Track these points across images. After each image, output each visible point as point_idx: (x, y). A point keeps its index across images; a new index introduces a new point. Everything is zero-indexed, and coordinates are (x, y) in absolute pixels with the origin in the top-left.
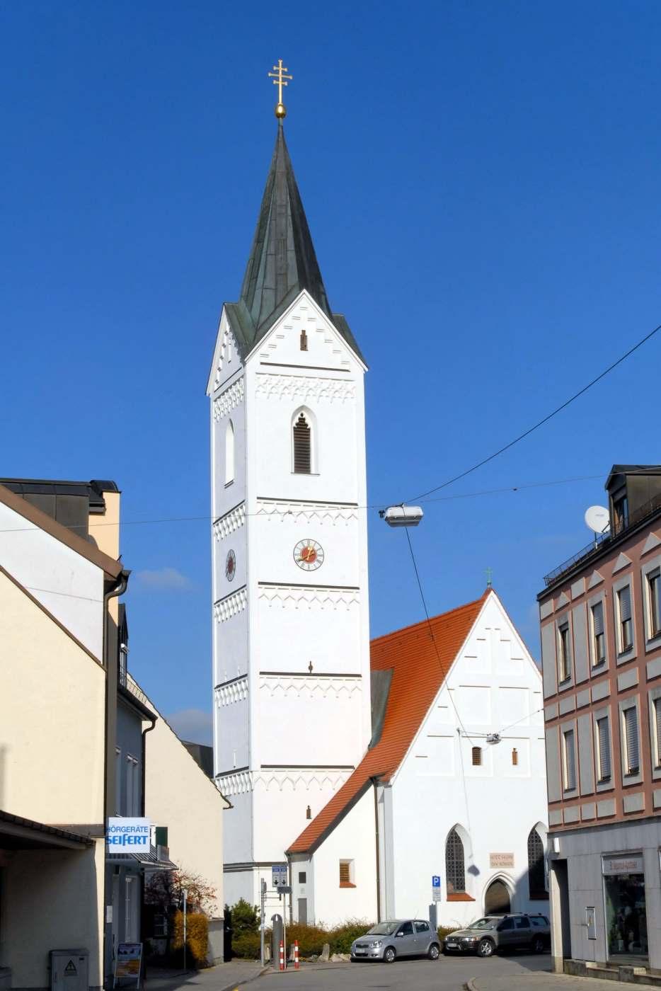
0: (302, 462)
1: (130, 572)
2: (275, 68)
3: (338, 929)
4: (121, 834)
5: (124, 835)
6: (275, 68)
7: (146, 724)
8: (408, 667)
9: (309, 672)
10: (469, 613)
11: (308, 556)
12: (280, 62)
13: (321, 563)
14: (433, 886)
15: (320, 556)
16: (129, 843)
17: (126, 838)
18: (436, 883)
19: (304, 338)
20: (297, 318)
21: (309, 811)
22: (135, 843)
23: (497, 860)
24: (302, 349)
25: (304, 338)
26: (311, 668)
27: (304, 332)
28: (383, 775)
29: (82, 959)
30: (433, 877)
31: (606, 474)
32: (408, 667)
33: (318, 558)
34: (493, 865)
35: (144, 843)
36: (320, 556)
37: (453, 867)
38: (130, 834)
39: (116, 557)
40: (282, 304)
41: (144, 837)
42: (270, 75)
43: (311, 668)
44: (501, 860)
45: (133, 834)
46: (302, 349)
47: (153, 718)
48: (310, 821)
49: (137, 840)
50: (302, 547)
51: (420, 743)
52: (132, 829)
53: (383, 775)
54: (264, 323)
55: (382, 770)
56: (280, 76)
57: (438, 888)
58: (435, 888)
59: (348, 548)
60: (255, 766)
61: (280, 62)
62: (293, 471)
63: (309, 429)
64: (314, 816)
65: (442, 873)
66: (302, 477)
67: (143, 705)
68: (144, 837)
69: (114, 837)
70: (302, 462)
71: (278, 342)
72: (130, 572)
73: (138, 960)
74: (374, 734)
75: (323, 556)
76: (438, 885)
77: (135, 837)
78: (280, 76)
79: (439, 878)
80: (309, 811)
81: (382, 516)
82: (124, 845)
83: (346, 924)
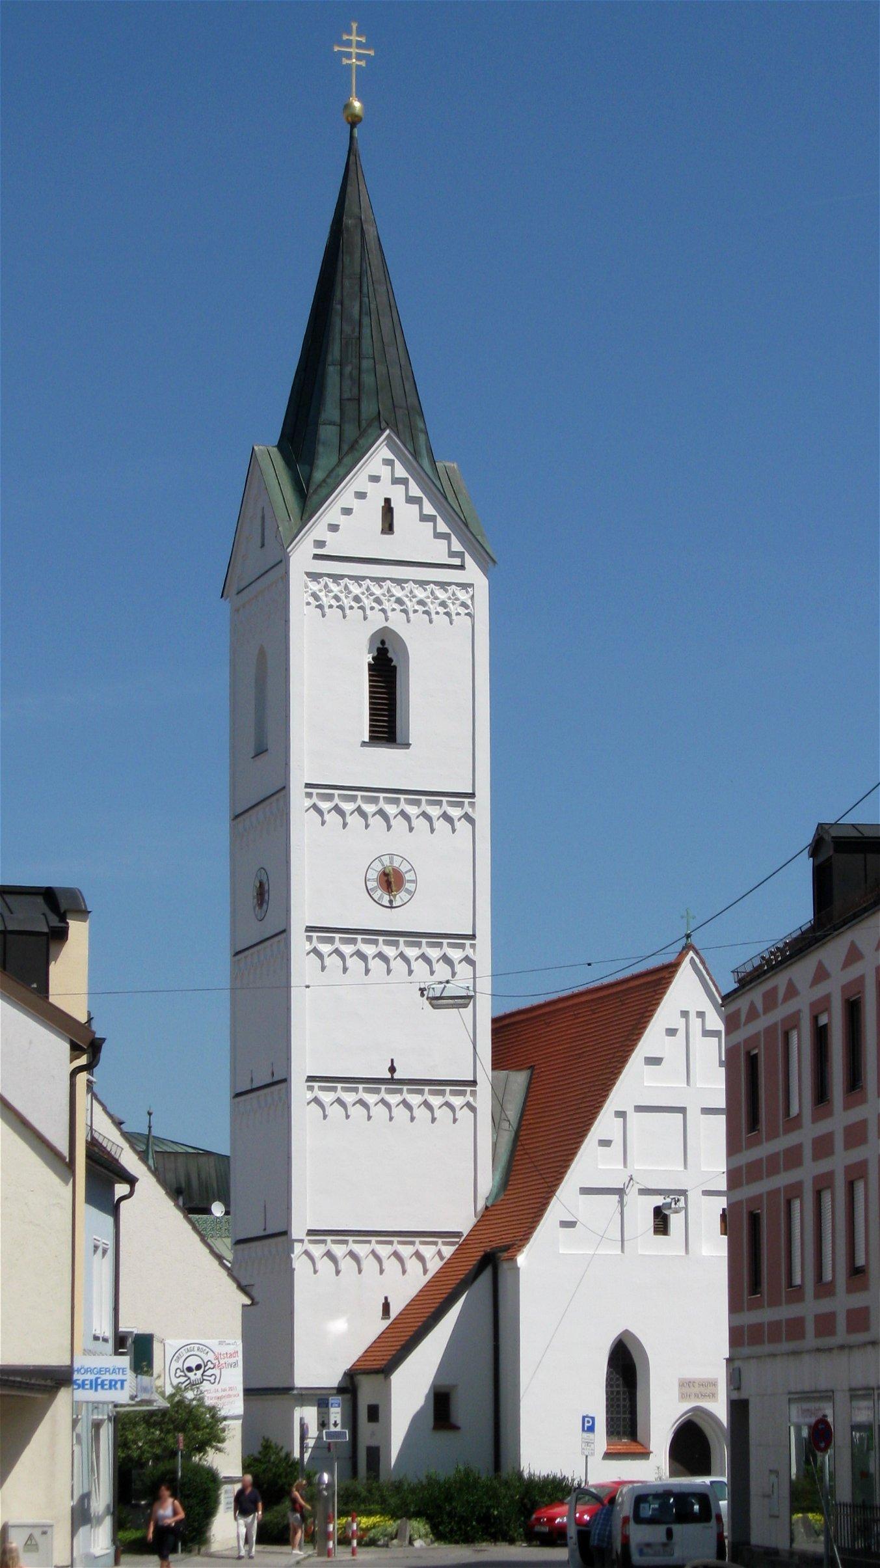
0: (386, 726)
1: (104, 1040)
2: (345, 37)
3: (554, 1477)
4: (93, 1377)
5: (97, 1379)
6: (345, 37)
7: (121, 1189)
8: (557, 1060)
9: (389, 1076)
10: (670, 969)
11: (391, 881)
12: (354, 26)
13: (411, 894)
14: (583, 1430)
15: (409, 881)
16: (102, 1388)
17: (99, 1381)
18: (589, 1427)
19: (388, 510)
20: (375, 479)
21: (386, 1307)
22: (110, 1388)
23: (687, 1387)
24: (383, 532)
25: (388, 510)
26: (392, 1069)
27: (388, 501)
28: (507, 1248)
29: (44, 1533)
30: (584, 1418)
31: (808, 837)
32: (557, 1060)
33: (408, 886)
34: (683, 1397)
35: (122, 1387)
36: (409, 881)
37: (618, 1400)
38: (104, 1377)
39: (82, 1018)
40: (352, 452)
41: (123, 1382)
42: (336, 49)
43: (392, 1069)
44: (696, 1390)
45: (107, 1377)
46: (383, 532)
47: (131, 1181)
48: (387, 1323)
49: (112, 1385)
50: (379, 868)
51: (566, 1198)
52: (107, 1370)
53: (507, 1248)
54: (319, 486)
55: (506, 1242)
56: (354, 50)
57: (590, 1435)
58: (585, 1435)
59: (453, 877)
60: (298, 1231)
61: (354, 26)
62: (367, 740)
63: (395, 667)
64: (394, 1312)
65: (599, 1411)
66: (384, 753)
67: (117, 1160)
68: (123, 1382)
69: (84, 1381)
70: (386, 726)
71: (342, 520)
72: (104, 1040)
73: (714, 1384)
74: (497, 1178)
75: (415, 881)
76: (591, 1429)
77: (111, 1381)
78: (354, 50)
79: (593, 1419)
80: (386, 1307)
81: (422, 995)
82: (96, 1390)
83: (559, 1475)
